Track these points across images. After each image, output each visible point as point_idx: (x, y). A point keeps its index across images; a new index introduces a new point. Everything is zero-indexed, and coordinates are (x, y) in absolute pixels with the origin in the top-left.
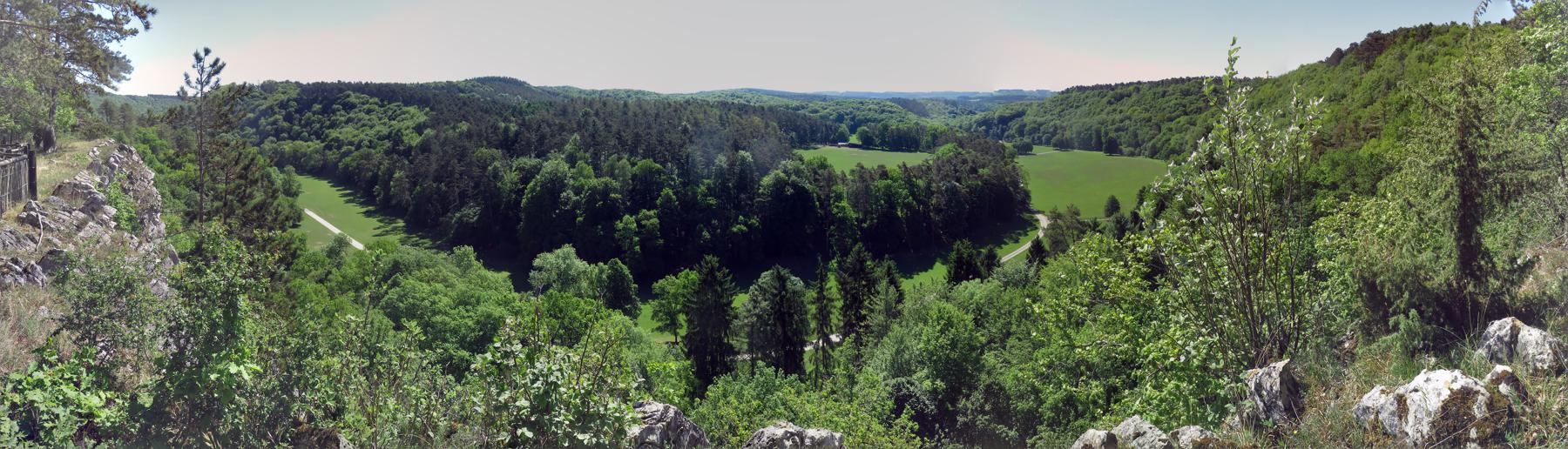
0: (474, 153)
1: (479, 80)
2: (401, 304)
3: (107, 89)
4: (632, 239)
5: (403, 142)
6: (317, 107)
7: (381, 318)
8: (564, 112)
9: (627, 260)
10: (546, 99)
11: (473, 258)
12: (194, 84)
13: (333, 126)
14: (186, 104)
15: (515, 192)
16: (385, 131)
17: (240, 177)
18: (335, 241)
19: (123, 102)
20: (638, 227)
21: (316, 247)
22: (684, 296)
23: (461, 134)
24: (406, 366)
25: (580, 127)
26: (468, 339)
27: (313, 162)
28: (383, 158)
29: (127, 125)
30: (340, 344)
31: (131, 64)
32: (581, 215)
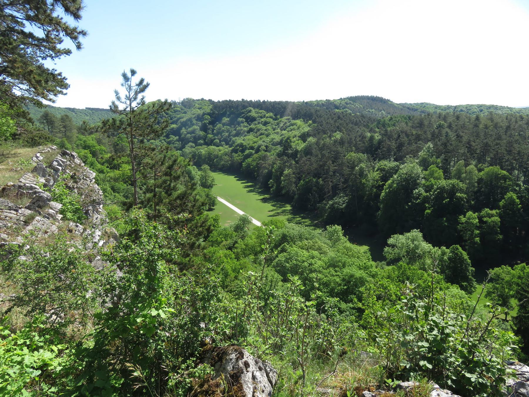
0: (345, 156)
1: (351, 99)
2: (287, 265)
3: (45, 102)
4: (473, 232)
5: (291, 147)
6: (226, 120)
7: (273, 273)
8: (421, 124)
9: (467, 247)
10: (406, 113)
11: (341, 234)
12: (123, 100)
13: (238, 134)
14: (118, 117)
15: (376, 187)
16: (277, 138)
17: (166, 174)
18: (240, 220)
19: (63, 114)
20: (479, 222)
21: (226, 224)
22: (518, 285)
23: (335, 141)
24: (290, 306)
25: (434, 137)
26: (336, 290)
27: (223, 163)
28: (276, 159)
29: (68, 134)
30: (244, 291)
31: (67, 81)
32: (429, 208)
